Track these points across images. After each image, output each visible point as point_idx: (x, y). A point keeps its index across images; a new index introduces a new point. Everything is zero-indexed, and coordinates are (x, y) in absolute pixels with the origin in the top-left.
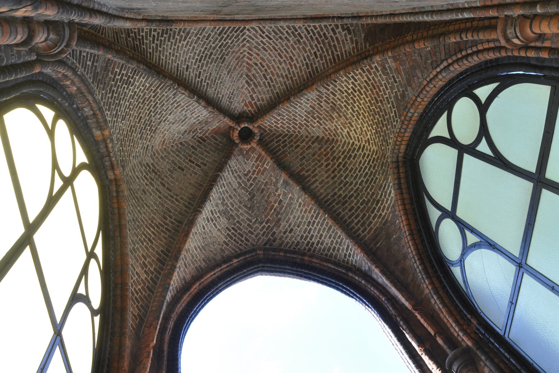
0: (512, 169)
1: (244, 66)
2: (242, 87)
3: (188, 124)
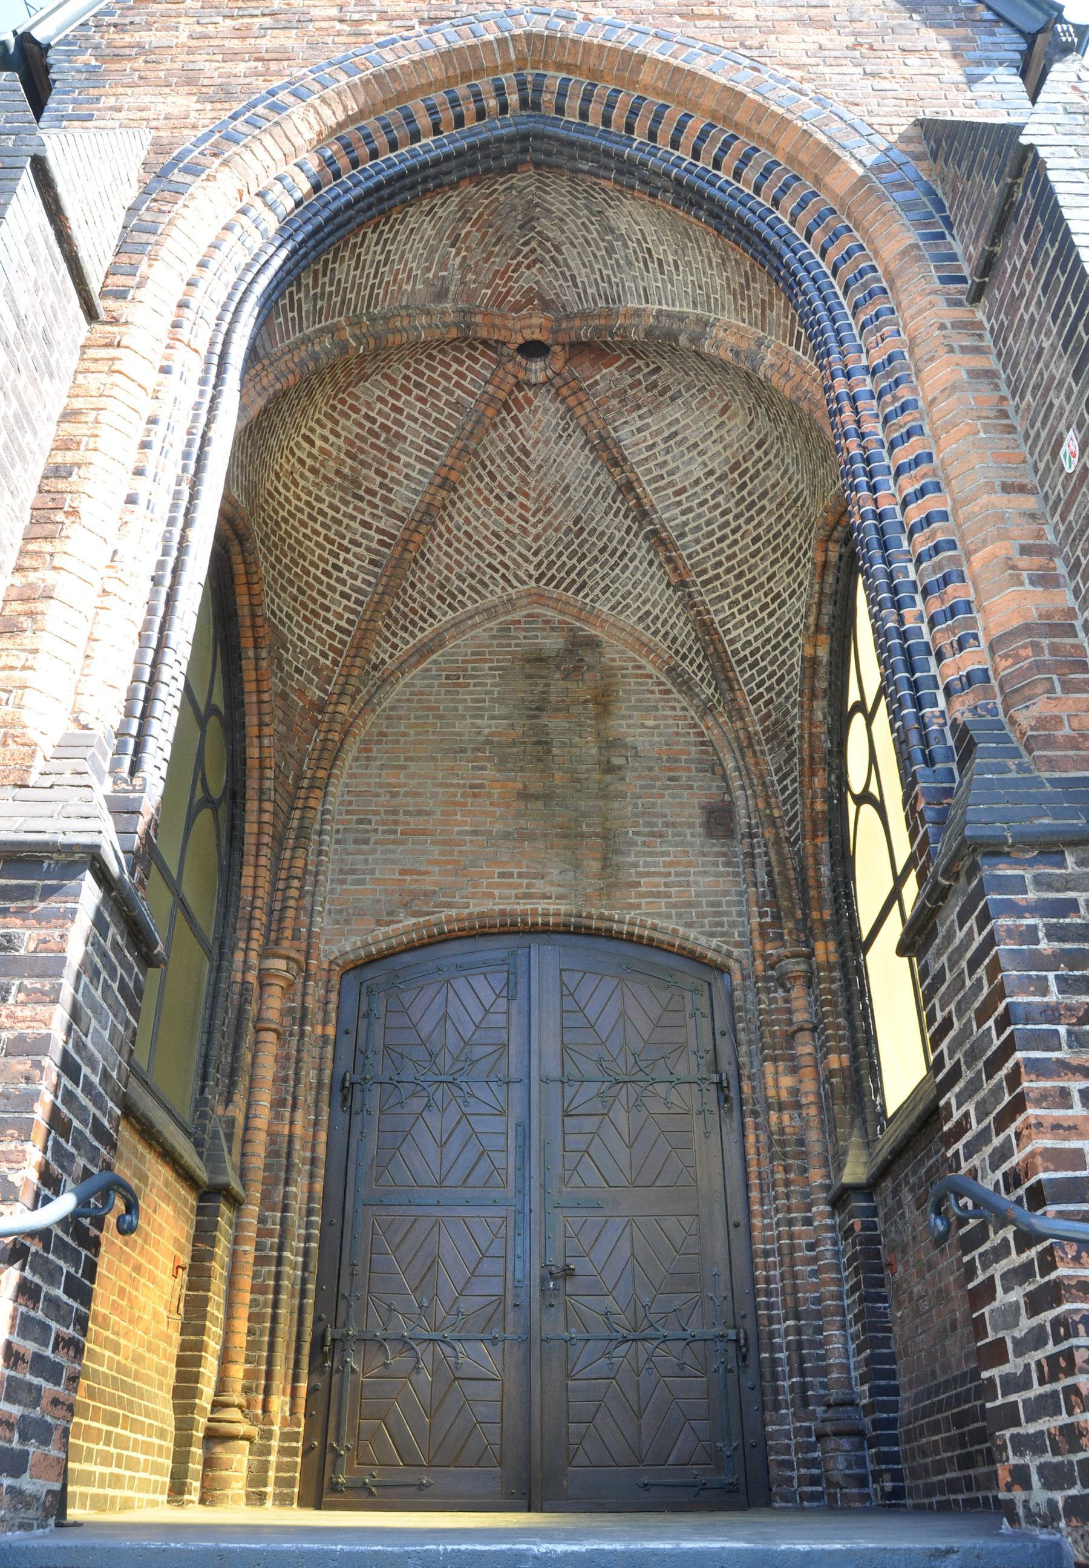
0: (225, 915)
1: (534, 490)
2: (536, 443)
3: (664, 418)
